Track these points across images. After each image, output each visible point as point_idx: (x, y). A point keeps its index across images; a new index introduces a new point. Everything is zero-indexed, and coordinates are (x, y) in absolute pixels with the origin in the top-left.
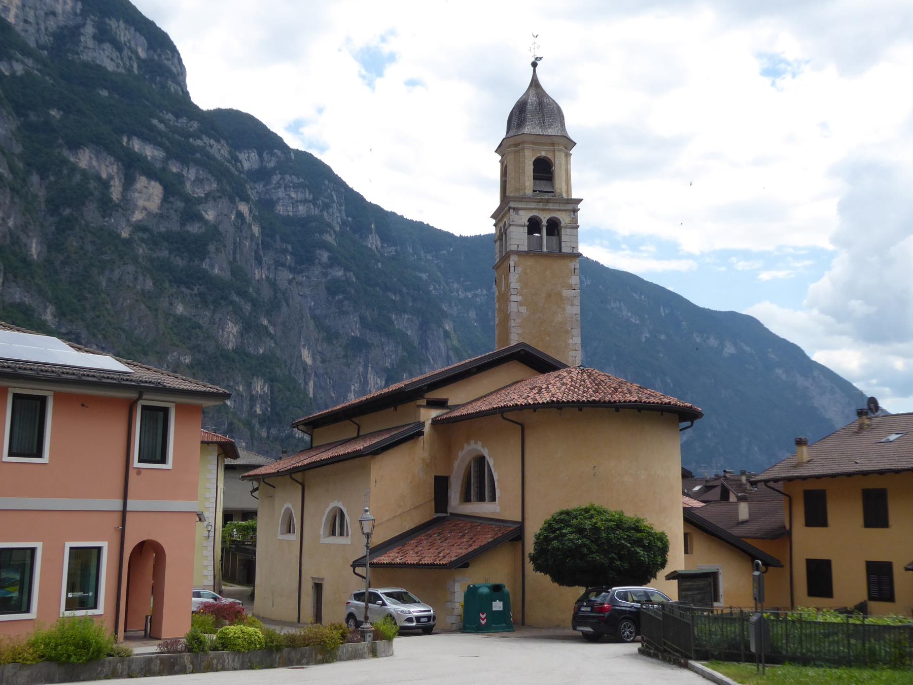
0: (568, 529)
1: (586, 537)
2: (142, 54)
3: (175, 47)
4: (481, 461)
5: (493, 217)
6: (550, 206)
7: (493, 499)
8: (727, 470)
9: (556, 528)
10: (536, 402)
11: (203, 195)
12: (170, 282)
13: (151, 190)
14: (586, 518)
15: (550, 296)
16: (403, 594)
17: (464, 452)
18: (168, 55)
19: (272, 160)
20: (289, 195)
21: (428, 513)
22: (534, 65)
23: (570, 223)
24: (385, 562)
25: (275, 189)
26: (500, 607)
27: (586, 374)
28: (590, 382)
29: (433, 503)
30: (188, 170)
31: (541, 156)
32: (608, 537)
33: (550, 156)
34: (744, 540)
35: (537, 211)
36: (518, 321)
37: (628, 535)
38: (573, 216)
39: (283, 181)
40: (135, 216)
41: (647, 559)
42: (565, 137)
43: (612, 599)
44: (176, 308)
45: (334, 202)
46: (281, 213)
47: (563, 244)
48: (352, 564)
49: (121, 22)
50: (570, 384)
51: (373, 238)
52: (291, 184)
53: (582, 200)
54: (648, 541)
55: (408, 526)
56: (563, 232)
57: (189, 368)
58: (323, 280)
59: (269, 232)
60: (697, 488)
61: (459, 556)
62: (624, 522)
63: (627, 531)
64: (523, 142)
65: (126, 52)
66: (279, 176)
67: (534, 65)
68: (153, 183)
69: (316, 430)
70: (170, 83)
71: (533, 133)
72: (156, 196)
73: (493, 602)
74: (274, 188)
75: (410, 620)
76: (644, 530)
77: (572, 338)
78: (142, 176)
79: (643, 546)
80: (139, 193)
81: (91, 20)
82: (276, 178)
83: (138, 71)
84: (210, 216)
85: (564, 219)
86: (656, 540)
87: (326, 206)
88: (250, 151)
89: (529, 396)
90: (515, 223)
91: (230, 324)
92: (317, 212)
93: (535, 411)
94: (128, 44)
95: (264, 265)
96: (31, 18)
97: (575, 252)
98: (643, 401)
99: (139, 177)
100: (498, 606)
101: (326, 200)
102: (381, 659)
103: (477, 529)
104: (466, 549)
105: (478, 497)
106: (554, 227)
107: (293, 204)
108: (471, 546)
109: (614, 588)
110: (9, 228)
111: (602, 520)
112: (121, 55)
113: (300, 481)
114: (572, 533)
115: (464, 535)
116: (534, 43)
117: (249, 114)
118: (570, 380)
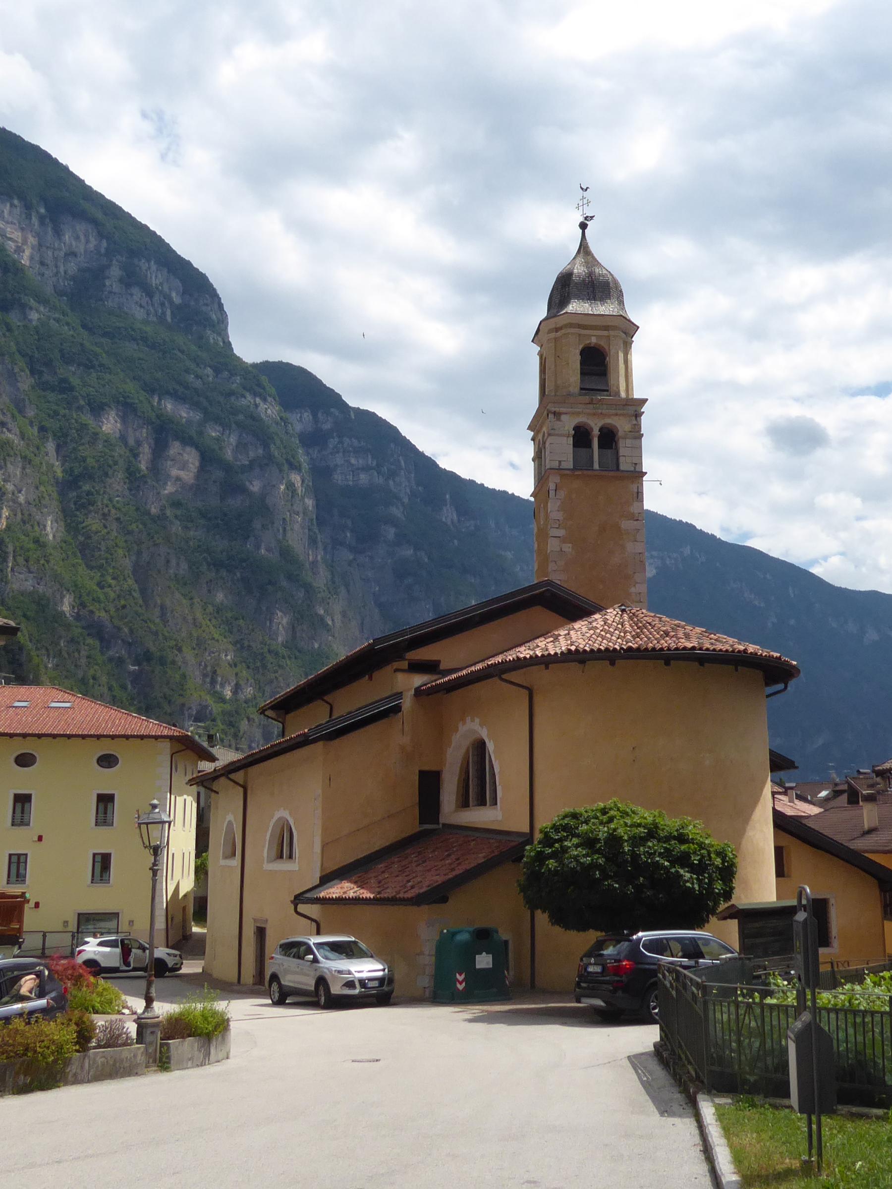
0: (574, 839)
1: (598, 852)
2: (177, 299)
3: (214, 290)
4: (480, 747)
5: (530, 428)
7: (494, 803)
8: (861, 770)
9: (555, 839)
10: (546, 653)
11: (247, 463)
12: (209, 564)
13: (186, 457)
14: (601, 823)
16: (352, 944)
17: (458, 735)
18: (207, 300)
19: (328, 420)
20: (348, 461)
21: (411, 825)
22: (583, 226)
23: (631, 432)
24: (334, 897)
25: (332, 455)
26: (488, 963)
27: (628, 615)
28: (630, 625)
29: (417, 811)
30: (230, 434)
31: (590, 343)
32: (634, 851)
33: (602, 343)
34: (866, 855)
37: (665, 848)
38: (635, 422)
39: (341, 445)
40: (168, 488)
41: (696, 887)
42: (624, 317)
43: (634, 952)
44: (216, 596)
45: (402, 469)
46: (339, 482)
47: (621, 459)
48: (293, 899)
49: (152, 262)
50: (601, 629)
51: (447, 510)
52: (351, 449)
53: (647, 400)
54: (699, 857)
55: (378, 844)
56: (621, 443)
57: (231, 667)
58: (389, 561)
59: (325, 506)
60: (824, 794)
61: (432, 886)
62: (662, 827)
63: (664, 842)
65: (156, 298)
66: (337, 440)
67: (583, 226)
68: (188, 449)
69: (289, 717)
70: (209, 332)
71: (579, 312)
72: (192, 463)
73: (477, 956)
74: (331, 453)
75: (350, 984)
76: (692, 839)
77: (634, 586)
78: (175, 440)
79: (693, 869)
80: (172, 460)
81: (117, 261)
82: (333, 442)
83: (172, 319)
84: (255, 487)
85: (622, 425)
86: (713, 856)
87: (392, 474)
88: (303, 411)
89: (538, 646)
90: (557, 432)
91: (280, 614)
92: (381, 481)
93: (547, 668)
94: (160, 288)
95: (320, 545)
96: (49, 260)
98: (704, 648)
99: (172, 441)
100: (484, 961)
101: (393, 467)
102: (176, 1074)
103: (470, 845)
104: (445, 875)
105: (478, 800)
106: (609, 438)
107: (353, 471)
108: (453, 870)
109: (640, 934)
110: (20, 504)
111: (626, 824)
112: (151, 301)
113: (241, 783)
114: (577, 846)
115: (449, 855)
116: (583, 198)
117: (302, 367)
118: (602, 623)
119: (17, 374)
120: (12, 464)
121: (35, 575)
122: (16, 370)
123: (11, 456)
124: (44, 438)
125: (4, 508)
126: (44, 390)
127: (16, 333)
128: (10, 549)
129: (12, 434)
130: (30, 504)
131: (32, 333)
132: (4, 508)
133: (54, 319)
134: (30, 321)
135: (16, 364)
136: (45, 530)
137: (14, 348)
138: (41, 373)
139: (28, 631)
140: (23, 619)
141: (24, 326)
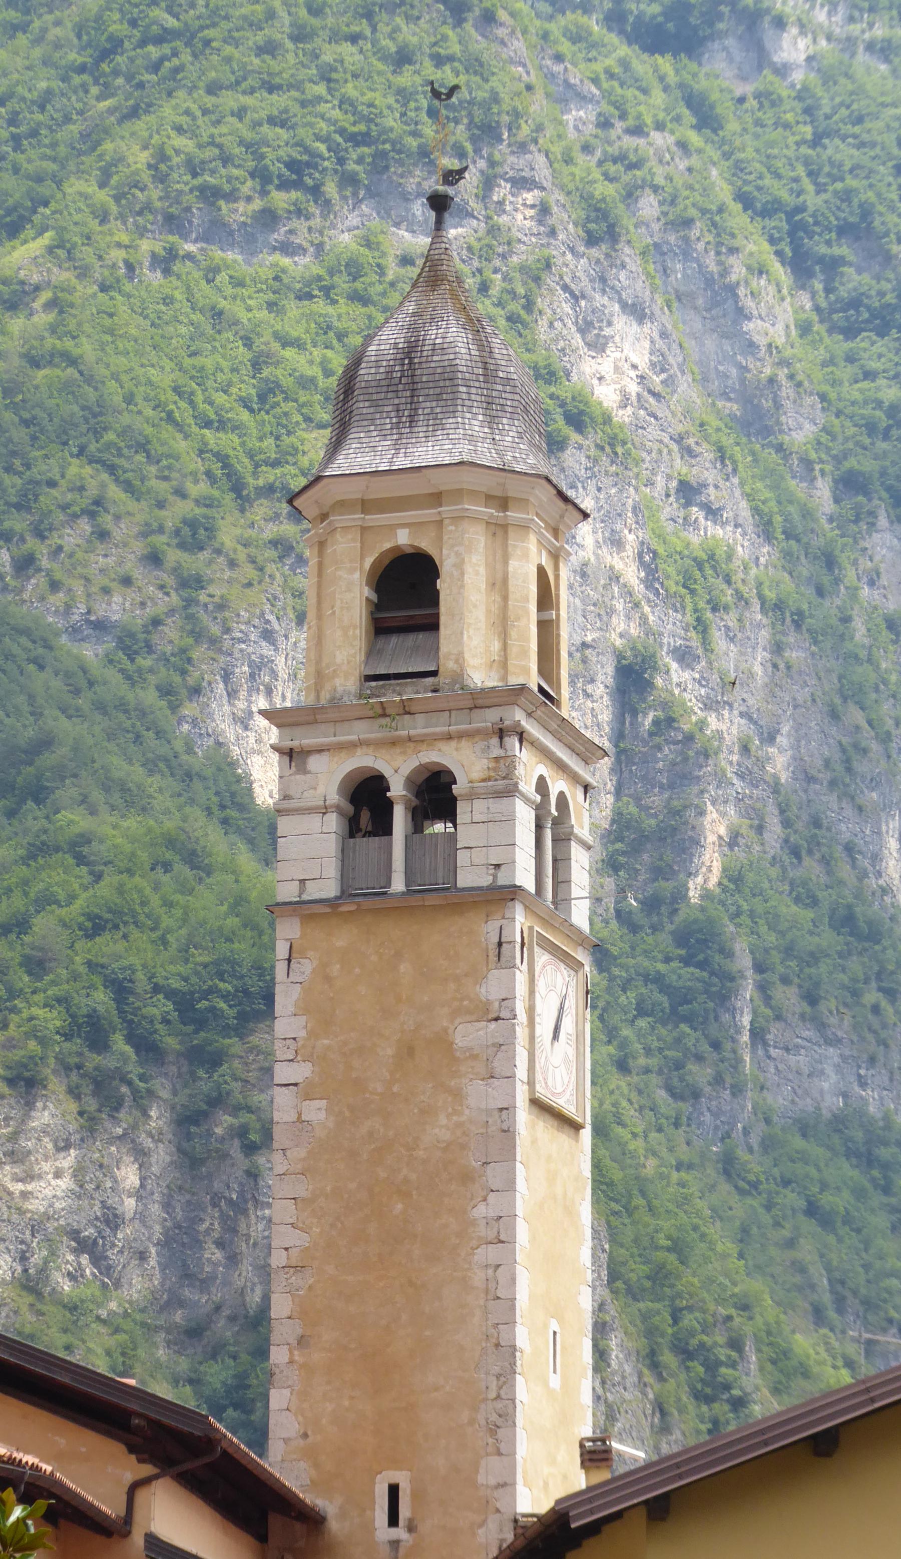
6: (418, 726)
15: (411, 1051)
23: (488, 779)
33: (426, 544)
35: (370, 751)
36: (298, 1153)
38: (497, 752)
64: (458, 494)
77: (485, 1200)
97: (501, 882)
110: (776, 788)
119: (742, 291)
120: (732, 639)
121: (847, 1052)
122: (738, 271)
123: (726, 608)
124: (857, 521)
125: (710, 808)
126: (850, 332)
127: (732, 126)
128: (744, 961)
129: (723, 524)
130: (810, 779)
131: (789, 117)
132: (710, 808)
133: (870, 47)
134: (782, 71)
135: (733, 251)
136: (879, 874)
137: (724, 192)
138: (832, 266)
139: (829, 1268)
140: (809, 1226)
141: (758, 96)
